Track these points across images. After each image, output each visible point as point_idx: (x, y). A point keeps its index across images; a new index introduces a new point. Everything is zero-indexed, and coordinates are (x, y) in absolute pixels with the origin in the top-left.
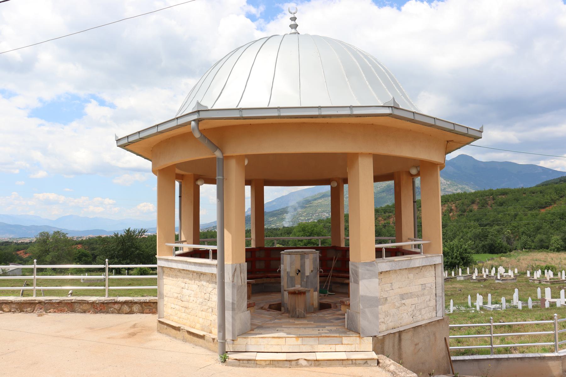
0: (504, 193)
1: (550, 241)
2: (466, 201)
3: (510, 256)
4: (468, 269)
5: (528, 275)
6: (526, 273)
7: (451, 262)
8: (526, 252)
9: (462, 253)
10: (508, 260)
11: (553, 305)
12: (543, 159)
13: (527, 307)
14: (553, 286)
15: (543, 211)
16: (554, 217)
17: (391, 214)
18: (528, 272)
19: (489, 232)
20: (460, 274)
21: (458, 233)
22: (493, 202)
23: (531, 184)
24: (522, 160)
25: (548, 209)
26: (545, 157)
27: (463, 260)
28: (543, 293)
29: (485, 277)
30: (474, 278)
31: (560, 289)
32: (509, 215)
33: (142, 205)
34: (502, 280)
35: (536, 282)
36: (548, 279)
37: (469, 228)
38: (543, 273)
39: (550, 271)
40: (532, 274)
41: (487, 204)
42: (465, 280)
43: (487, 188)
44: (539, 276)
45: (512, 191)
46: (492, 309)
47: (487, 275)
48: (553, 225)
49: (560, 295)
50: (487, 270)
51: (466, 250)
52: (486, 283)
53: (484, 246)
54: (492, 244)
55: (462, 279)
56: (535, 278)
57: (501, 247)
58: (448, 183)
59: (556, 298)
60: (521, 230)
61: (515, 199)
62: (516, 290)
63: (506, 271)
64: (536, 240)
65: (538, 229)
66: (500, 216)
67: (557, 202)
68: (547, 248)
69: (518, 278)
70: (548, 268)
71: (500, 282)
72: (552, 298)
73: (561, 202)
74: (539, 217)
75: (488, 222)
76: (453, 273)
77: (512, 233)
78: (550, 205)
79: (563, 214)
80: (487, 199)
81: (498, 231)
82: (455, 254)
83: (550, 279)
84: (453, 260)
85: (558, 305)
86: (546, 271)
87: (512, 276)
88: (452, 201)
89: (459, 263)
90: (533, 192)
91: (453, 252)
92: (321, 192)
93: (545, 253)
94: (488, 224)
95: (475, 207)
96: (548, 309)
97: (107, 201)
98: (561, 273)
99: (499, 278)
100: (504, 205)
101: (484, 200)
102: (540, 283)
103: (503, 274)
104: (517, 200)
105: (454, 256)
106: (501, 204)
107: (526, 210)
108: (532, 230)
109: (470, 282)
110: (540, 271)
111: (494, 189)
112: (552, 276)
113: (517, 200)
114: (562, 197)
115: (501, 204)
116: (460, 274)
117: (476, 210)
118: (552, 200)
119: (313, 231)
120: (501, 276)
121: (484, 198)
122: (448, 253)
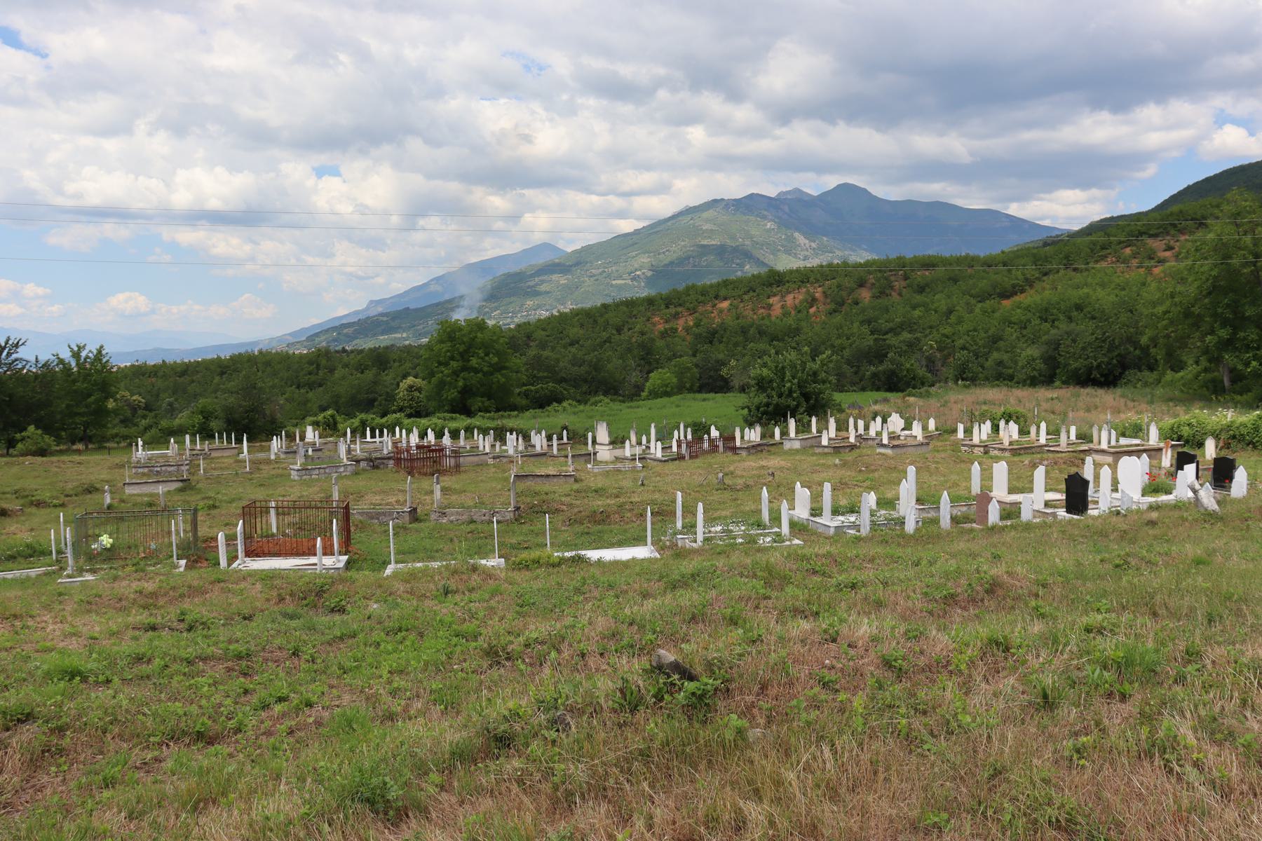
0: (929, 264)
1: (1016, 363)
2: (848, 283)
3: (928, 395)
4: (814, 420)
5: (960, 434)
6: (955, 431)
7: (777, 405)
8: (965, 386)
9: (806, 381)
10: (921, 402)
11: (1011, 512)
12: (1012, 200)
13: (935, 521)
14: (1016, 459)
15: (1006, 303)
16: (1029, 315)
17: (680, 309)
18: (961, 427)
19: (890, 347)
20: (792, 434)
21: (823, 348)
22: (903, 283)
23: (983, 250)
24: (972, 199)
25: (1016, 299)
26: (1021, 198)
27: (807, 400)
28: (987, 476)
29: (852, 440)
30: (825, 442)
31: (1034, 466)
32: (936, 312)
33: (121, 297)
34: (894, 447)
35: (976, 450)
36: (1006, 443)
37: (848, 339)
38: (996, 428)
39: (1011, 423)
40: (968, 431)
41: (892, 288)
42: (803, 450)
43: (893, 256)
44: (984, 437)
45: (946, 262)
46: (832, 531)
47: (858, 437)
48: (1025, 332)
49: (1032, 482)
50: (861, 423)
51: (815, 374)
52: (850, 456)
53: (875, 375)
54: (893, 373)
55: (797, 445)
56: (976, 440)
57: (914, 378)
58: (814, 245)
59: (1021, 491)
60: (959, 343)
61: (950, 279)
62: (911, 470)
63: (908, 427)
64: (988, 364)
65: (995, 340)
66: (917, 313)
67: (1038, 285)
68: (1011, 378)
69: (933, 443)
70: (1008, 417)
71: (889, 451)
72: (1011, 491)
73: (1044, 284)
74: (997, 315)
75: (891, 325)
76: (777, 431)
77: (940, 350)
78: (1022, 291)
79: (1046, 310)
80: (893, 278)
81: (910, 345)
82: (788, 385)
83: (1011, 444)
84: (782, 400)
85: (1026, 515)
86: (1002, 424)
87: (920, 438)
88: (817, 281)
89: (797, 406)
90: (989, 263)
91: (783, 380)
92: (533, 262)
93: (1005, 389)
94: (891, 330)
95: (865, 295)
96: (993, 528)
97: (30, 289)
98: (1038, 427)
99: (885, 441)
100: (928, 290)
101: (886, 279)
102: (986, 453)
103: (898, 431)
104: (955, 280)
105: (785, 390)
106: (921, 289)
107: (973, 301)
108: (981, 343)
109: (814, 454)
110: (988, 423)
111: (909, 254)
112: (1015, 436)
113: (955, 280)
114: (1046, 274)
115: (921, 289)
116: (792, 434)
117: (867, 301)
118: (1027, 279)
119: (473, 339)
120: (890, 438)
121: (882, 277)
122: (771, 381)
